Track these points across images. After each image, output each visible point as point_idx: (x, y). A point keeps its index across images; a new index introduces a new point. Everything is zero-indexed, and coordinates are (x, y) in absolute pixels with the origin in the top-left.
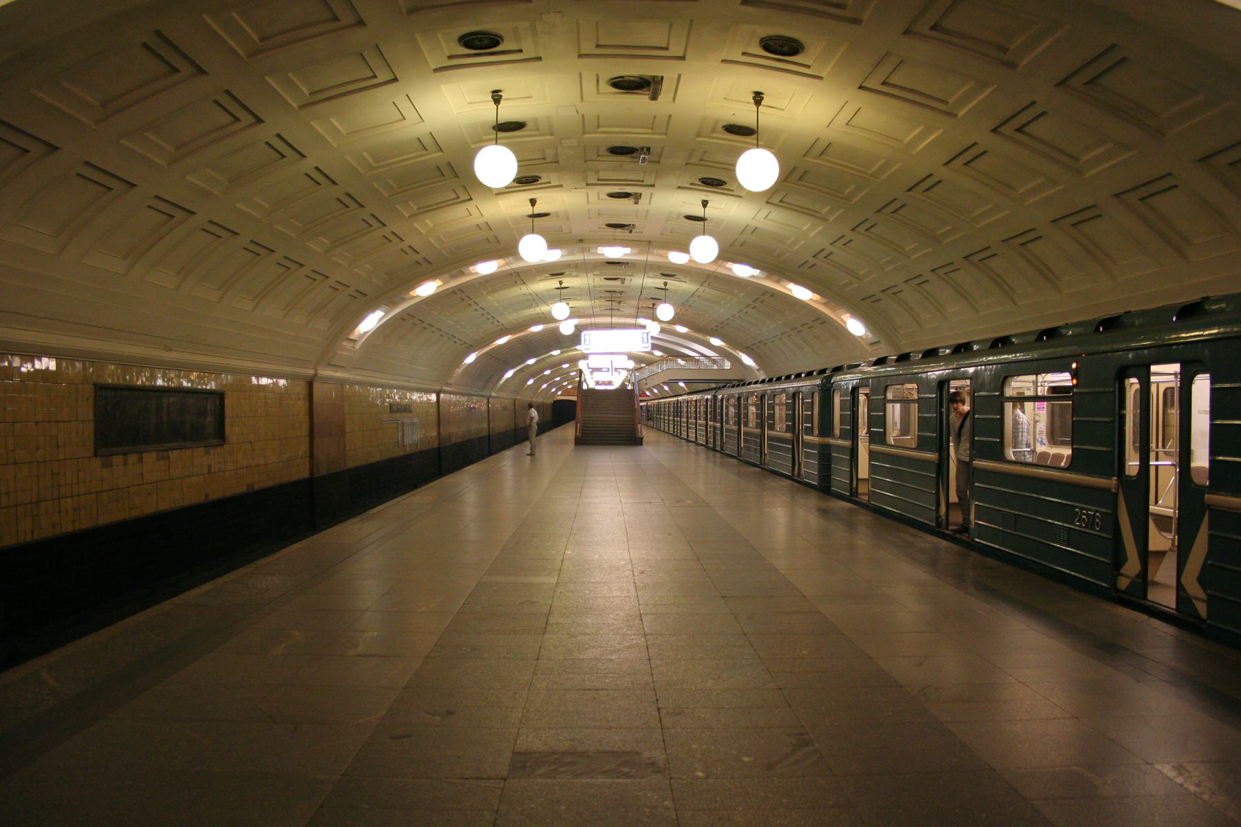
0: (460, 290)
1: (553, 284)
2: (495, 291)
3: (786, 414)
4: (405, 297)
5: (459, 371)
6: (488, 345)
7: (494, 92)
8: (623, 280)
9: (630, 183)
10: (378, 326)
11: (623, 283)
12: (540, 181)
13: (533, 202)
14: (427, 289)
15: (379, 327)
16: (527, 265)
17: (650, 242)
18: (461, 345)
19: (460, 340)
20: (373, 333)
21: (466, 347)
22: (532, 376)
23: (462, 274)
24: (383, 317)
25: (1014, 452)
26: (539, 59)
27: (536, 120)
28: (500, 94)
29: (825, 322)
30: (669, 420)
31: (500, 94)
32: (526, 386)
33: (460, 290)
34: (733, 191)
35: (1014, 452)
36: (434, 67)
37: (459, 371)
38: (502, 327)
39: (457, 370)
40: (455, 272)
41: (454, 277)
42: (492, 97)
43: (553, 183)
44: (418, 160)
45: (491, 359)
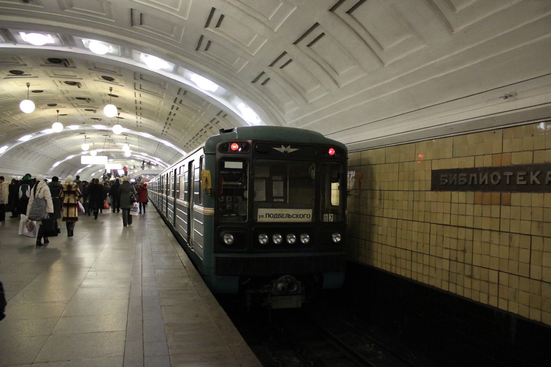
0: (39, 139)
1: (82, 136)
2: (58, 139)
3: (217, 260)
4: (17, 141)
5: (52, 169)
6: (64, 159)
7: (27, 83)
8: (110, 136)
9: (93, 107)
10: (6, 151)
11: (110, 137)
12: (57, 106)
13: (58, 111)
14: (25, 138)
15: (6, 153)
16: (23, 142)
17: (109, 124)
18: (50, 159)
19: (49, 157)
20: (3, 155)
21: (53, 160)
22: (93, 172)
23: (40, 133)
24: (8, 148)
25: (185, 16)
26: (37, 77)
27: (46, 90)
28: (29, 84)
29: (226, 115)
30: (167, 200)
31: (29, 84)
32: (91, 176)
33: (42, 138)
34: (381, 48)
35: (185, 16)
36: (4, 77)
37: (52, 169)
38: (68, 152)
39: (50, 169)
40: (37, 132)
41: (37, 134)
42: (27, 85)
43: (62, 106)
44: (4, 100)
45: (67, 164)
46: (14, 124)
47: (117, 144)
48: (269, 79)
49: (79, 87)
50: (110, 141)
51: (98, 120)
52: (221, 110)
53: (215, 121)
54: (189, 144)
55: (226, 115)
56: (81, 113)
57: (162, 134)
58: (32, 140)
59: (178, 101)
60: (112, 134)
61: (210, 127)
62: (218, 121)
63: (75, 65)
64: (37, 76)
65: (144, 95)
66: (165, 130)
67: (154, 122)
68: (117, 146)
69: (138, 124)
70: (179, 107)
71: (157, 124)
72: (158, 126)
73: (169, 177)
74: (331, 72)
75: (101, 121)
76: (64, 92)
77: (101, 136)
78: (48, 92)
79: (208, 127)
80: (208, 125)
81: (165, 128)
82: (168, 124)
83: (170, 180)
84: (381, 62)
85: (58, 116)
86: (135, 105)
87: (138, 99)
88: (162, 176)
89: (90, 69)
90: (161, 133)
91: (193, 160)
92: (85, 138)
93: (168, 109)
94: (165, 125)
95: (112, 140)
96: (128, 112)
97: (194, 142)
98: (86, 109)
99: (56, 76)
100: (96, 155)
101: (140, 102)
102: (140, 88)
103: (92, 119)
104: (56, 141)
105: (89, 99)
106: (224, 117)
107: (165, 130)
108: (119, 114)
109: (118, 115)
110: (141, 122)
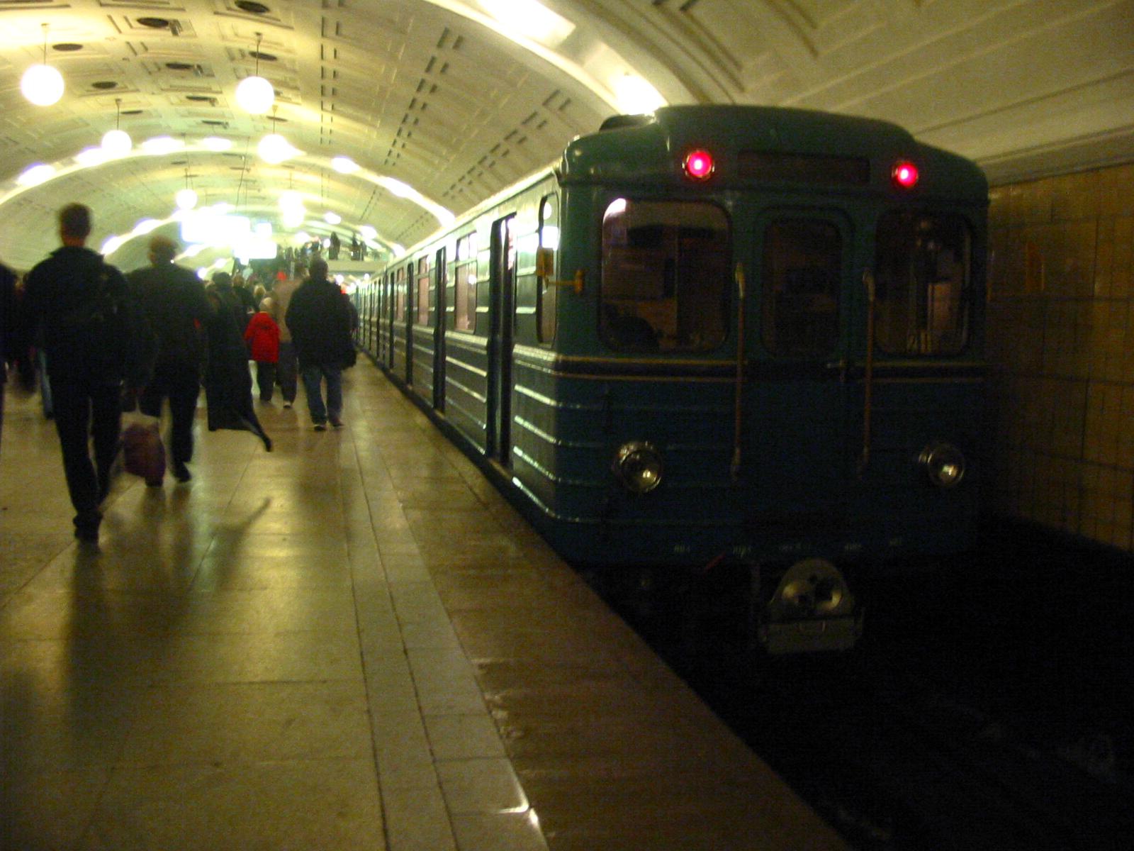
17: (249, 138)
23: (72, 163)
26: (67, 6)
29: (568, 102)
41: (65, 165)
46: (7, 138)
47: (264, 192)
48: (545, 122)
49: (175, 33)
50: (249, 184)
51: (216, 125)
52: (554, 89)
53: (517, 137)
54: (459, 187)
55: (568, 102)
56: (131, 40)
57: (386, 162)
58: (502, 408)
59: (438, 66)
60: (221, 92)
61: (502, 152)
62: (545, 122)
63: (193, 29)
64: (68, 3)
65: (337, 119)
66: (395, 151)
67: (366, 130)
68: (264, 198)
69: (324, 64)
70: (439, 83)
71: (374, 135)
72: (376, 137)
73: (416, 272)
74: (800, 20)
75: (228, 131)
76: (134, 47)
77: (225, 170)
78: (93, 49)
79: (515, 139)
80: (515, 132)
81: (397, 145)
82: (405, 133)
83: (419, 280)
84: (814, 52)
85: (118, 116)
86: (320, 64)
87: (328, 126)
88: (392, 275)
89: (216, 13)
90: (384, 160)
91: (426, 257)
92: (187, 176)
93: (388, 146)
94: (408, 112)
95: (254, 182)
96: (292, 22)
97: (461, 190)
98: (191, 94)
99: (173, 89)
100: (196, 207)
101: (335, 72)
102: (337, 33)
103: (207, 126)
104: (113, 184)
105: (199, 67)
106: (540, 126)
107: (395, 151)
108: (275, 108)
109: (272, 111)
110: (333, 129)
